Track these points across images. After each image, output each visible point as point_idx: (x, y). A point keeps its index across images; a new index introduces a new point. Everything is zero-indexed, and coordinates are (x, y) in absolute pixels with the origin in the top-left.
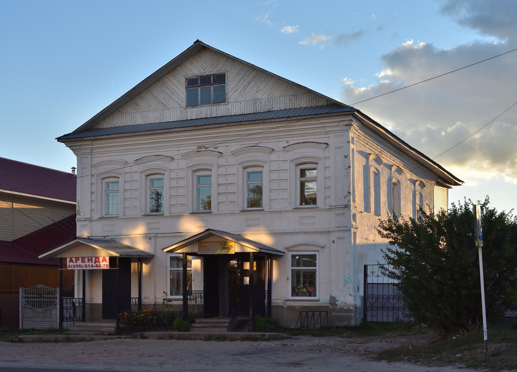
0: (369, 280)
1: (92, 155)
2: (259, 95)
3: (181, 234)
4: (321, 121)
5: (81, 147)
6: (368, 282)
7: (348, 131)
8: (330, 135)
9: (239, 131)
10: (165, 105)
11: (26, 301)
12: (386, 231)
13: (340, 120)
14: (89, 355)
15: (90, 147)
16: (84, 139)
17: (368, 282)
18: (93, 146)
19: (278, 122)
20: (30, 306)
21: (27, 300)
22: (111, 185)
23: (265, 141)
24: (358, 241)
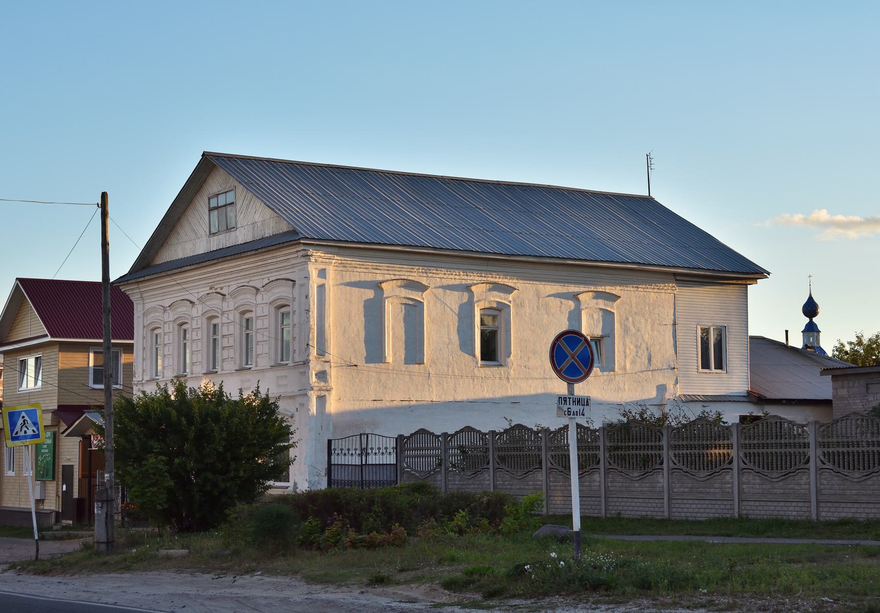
0: (335, 460)
1: (143, 300)
2: (258, 218)
4: (284, 252)
5: (134, 292)
6: (333, 463)
7: (306, 263)
8: (296, 269)
9: (233, 267)
10: (196, 233)
11: (675, 455)
13: (295, 250)
15: (138, 291)
16: (129, 282)
17: (333, 463)
18: (142, 290)
19: (252, 255)
21: (747, 451)
23: (255, 278)
24: (333, 406)
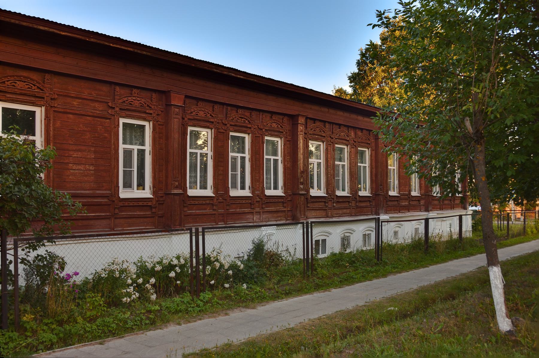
3: (362, 121)
12: (13, 137)
14: (277, 241)
20: (394, 191)
22: (534, 214)
